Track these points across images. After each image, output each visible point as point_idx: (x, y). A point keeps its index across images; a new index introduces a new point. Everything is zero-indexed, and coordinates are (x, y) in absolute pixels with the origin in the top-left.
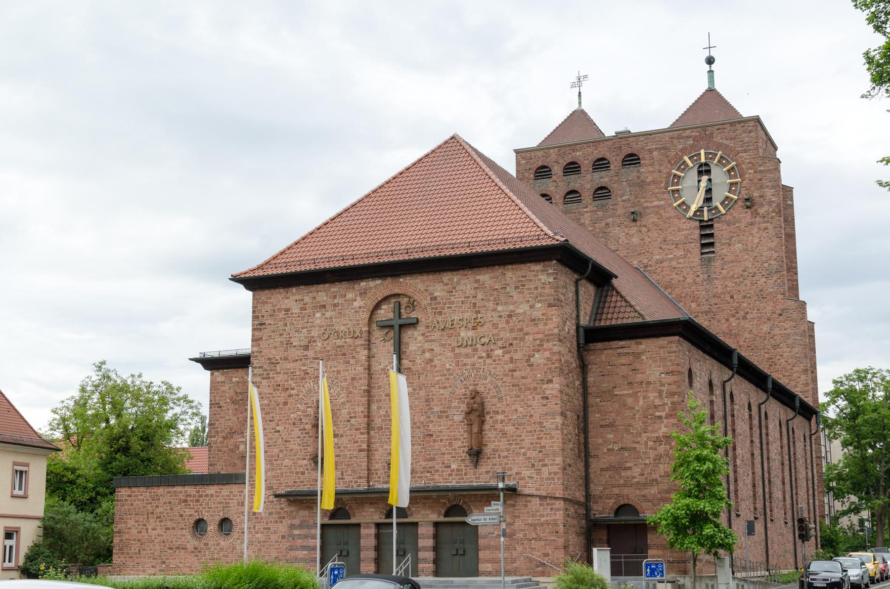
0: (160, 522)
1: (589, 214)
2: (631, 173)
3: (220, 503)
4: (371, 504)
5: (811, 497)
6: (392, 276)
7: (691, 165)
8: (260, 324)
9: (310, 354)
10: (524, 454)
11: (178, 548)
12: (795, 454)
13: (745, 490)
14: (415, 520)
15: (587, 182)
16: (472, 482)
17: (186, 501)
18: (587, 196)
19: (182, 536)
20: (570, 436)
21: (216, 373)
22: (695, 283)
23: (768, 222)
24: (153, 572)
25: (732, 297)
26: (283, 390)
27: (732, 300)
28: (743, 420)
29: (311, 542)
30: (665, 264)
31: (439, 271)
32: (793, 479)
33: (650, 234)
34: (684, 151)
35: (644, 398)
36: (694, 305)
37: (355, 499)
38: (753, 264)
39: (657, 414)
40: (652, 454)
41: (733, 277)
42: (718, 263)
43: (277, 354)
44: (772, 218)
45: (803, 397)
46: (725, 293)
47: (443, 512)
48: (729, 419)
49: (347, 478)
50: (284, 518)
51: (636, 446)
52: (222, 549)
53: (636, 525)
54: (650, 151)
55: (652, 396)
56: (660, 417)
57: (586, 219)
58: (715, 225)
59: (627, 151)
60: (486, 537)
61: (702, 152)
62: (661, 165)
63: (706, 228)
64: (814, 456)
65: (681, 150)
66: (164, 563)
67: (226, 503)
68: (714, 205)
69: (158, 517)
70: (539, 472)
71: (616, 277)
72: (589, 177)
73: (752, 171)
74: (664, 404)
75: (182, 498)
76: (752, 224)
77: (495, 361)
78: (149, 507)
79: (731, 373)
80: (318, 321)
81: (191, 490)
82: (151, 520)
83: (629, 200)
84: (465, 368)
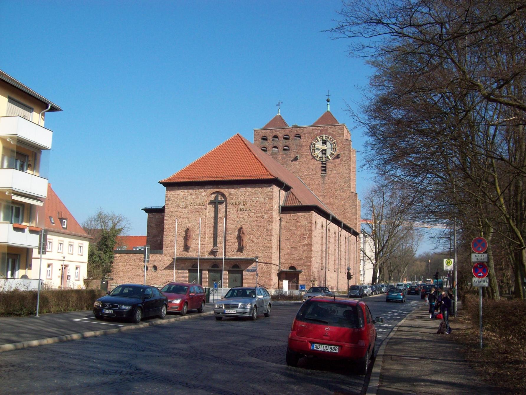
2: (297, 141)
9: (186, 210)
13: (332, 262)
15: (281, 143)
18: (281, 149)
22: (318, 184)
29: (185, 275)
30: (308, 176)
34: (317, 135)
36: (318, 192)
40: (302, 250)
42: (327, 178)
43: (173, 210)
45: (354, 229)
48: (328, 238)
54: (305, 134)
55: (303, 230)
57: (280, 157)
58: (327, 163)
59: (296, 133)
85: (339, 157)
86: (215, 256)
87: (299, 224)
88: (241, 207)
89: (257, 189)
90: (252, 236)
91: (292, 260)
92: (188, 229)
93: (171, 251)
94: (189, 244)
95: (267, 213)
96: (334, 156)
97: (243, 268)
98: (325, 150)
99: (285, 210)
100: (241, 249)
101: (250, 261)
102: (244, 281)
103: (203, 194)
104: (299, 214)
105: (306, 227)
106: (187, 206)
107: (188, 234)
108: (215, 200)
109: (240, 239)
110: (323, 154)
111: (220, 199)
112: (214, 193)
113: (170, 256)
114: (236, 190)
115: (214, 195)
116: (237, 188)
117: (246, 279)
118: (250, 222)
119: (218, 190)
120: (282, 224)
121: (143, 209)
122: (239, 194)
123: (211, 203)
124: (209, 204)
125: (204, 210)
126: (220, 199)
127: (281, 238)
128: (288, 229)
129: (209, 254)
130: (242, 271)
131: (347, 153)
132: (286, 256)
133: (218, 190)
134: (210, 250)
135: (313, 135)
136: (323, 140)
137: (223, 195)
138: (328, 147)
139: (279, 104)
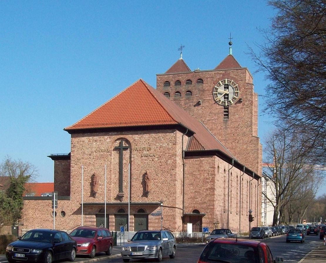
1: (183, 101)
2: (200, 86)
5: (256, 207)
7: (222, 84)
9: (92, 157)
10: (164, 193)
12: (252, 192)
15: (183, 88)
19: (48, 216)
20: (179, 188)
21: (56, 161)
23: (248, 108)
25: (234, 135)
27: (234, 136)
28: (235, 182)
29: (93, 220)
30: (211, 121)
32: (251, 201)
33: (205, 110)
34: (219, 79)
35: (203, 175)
36: (220, 137)
38: (242, 123)
39: (207, 181)
40: (205, 194)
41: (234, 127)
43: (79, 156)
44: (250, 106)
46: (231, 133)
47: (137, 211)
51: (200, 191)
52: (61, 221)
53: (190, 216)
54: (207, 78)
55: (206, 175)
56: (208, 182)
57: (182, 103)
59: (198, 77)
60: (151, 219)
62: (211, 84)
63: (226, 108)
64: (258, 193)
65: (218, 79)
66: (42, 225)
69: (39, 210)
71: (195, 133)
72: (184, 87)
73: (243, 88)
74: (209, 178)
76: (242, 108)
77: (155, 162)
78: (36, 207)
79: (232, 166)
82: (37, 211)
83: (198, 96)
84: (145, 164)
85: (241, 102)
86: (121, 201)
87: (202, 169)
88: (145, 152)
89: (160, 135)
92: (94, 175)
93: (78, 197)
95: (170, 158)
96: (236, 101)
97: (148, 212)
98: (228, 95)
99: (188, 155)
100: (146, 194)
103: (108, 140)
104: (202, 159)
106: (92, 152)
107: (94, 180)
108: (120, 146)
109: (144, 184)
110: (225, 98)
111: (124, 145)
112: (118, 139)
114: (140, 136)
115: (118, 142)
116: (141, 134)
118: (155, 167)
120: (186, 169)
121: (49, 157)
122: (143, 140)
123: (116, 149)
124: (114, 150)
125: (109, 157)
126: (124, 145)
127: (185, 182)
128: (192, 174)
129: (115, 199)
130: (148, 215)
131: (249, 97)
134: (116, 196)
135: (215, 80)
136: (225, 85)
137: (127, 141)
138: (230, 91)
139: (181, 48)
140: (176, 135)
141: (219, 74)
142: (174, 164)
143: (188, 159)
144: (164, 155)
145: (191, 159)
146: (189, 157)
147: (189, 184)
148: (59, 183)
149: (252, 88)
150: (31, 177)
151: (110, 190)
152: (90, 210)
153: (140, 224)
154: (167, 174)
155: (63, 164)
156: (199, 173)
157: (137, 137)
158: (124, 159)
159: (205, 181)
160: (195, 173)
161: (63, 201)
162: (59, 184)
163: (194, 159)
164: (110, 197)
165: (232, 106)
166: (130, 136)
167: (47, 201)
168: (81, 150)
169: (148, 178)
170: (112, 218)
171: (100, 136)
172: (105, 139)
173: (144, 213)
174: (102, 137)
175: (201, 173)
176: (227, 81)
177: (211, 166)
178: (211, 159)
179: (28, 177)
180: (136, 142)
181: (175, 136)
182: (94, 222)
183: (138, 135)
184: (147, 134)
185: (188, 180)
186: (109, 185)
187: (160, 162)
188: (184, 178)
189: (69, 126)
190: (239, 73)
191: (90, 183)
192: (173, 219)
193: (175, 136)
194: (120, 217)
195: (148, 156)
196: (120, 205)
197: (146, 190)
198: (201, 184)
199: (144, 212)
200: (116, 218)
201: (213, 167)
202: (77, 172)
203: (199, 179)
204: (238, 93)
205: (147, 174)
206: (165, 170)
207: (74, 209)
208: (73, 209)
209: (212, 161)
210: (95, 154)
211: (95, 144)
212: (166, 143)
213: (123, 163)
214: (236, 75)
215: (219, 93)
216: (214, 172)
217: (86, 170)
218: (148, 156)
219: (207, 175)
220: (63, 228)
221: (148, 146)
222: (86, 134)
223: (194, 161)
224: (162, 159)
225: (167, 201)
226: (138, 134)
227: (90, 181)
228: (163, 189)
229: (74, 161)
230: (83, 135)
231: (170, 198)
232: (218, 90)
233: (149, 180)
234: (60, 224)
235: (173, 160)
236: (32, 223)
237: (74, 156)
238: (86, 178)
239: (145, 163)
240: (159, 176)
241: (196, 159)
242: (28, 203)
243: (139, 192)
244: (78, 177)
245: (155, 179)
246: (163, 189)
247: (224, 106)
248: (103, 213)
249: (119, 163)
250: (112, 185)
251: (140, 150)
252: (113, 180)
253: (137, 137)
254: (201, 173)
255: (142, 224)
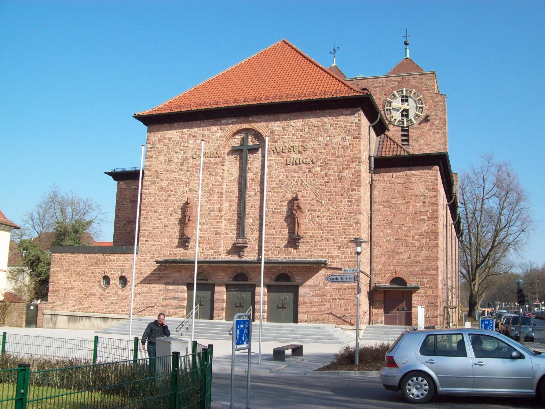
0: (79, 276)
3: (119, 266)
4: (223, 270)
6: (243, 116)
7: (398, 96)
8: (151, 148)
9: (185, 168)
11: (90, 294)
14: (253, 283)
16: (295, 258)
17: (96, 264)
21: (121, 183)
23: (439, 129)
24: (73, 310)
26: (164, 191)
29: (181, 295)
31: (277, 113)
34: (393, 88)
37: (212, 267)
39: (422, 217)
40: (417, 244)
43: (159, 167)
44: (441, 127)
47: (274, 277)
49: (207, 253)
50: (161, 277)
51: (407, 238)
52: (119, 297)
53: (385, 291)
54: (375, 87)
56: (424, 219)
61: (404, 89)
65: (392, 88)
66: (81, 304)
67: (123, 266)
68: (409, 118)
69: (78, 274)
70: (344, 252)
75: (94, 261)
76: (430, 130)
78: (72, 266)
80: (191, 146)
81: (101, 256)
82: (74, 275)
85: (429, 121)
86: (240, 256)
87: (410, 192)
88: (293, 156)
89: (326, 119)
90: (319, 213)
91: (398, 264)
92: (187, 203)
93: (153, 248)
94: (188, 232)
95: (348, 167)
96: (420, 120)
97: (298, 280)
98: (407, 111)
99: (382, 164)
100: (294, 241)
101: (312, 268)
102: (300, 308)
103: (218, 135)
104: (409, 173)
105: (426, 198)
106: (186, 158)
107: (187, 214)
108: (241, 145)
109: (292, 220)
110: (403, 116)
111: (250, 143)
112: (239, 132)
113: (152, 257)
114: (284, 123)
115: (239, 137)
116: (286, 120)
117: (304, 303)
118: (314, 185)
119: (247, 126)
120: (375, 193)
121: (109, 174)
122: (289, 131)
123: (234, 151)
124: (229, 153)
125: (220, 167)
126: (250, 143)
127: (374, 220)
128: (388, 203)
129: (229, 252)
130: (297, 287)
131: (440, 113)
132: (384, 257)
133: (247, 126)
134: (230, 245)
135: (387, 89)
136: (403, 97)
137: (258, 136)
138: (411, 105)
139: (334, 51)
140: (359, 120)
141: (393, 81)
142: (357, 178)
143: (380, 174)
144: (335, 161)
145: (387, 174)
146: (383, 169)
147: (382, 224)
148: (124, 224)
149: (444, 100)
150: (93, 224)
151: (219, 234)
152: (177, 275)
153: (237, 305)
154: (340, 200)
155: (133, 187)
156: (404, 202)
157: (278, 126)
158: (249, 171)
159: (417, 217)
160: (396, 202)
161: (125, 255)
162: (123, 225)
163: (394, 174)
164: (217, 247)
165: (414, 128)
166: (264, 124)
167: (93, 255)
168: (165, 155)
169: (299, 208)
170: (219, 292)
171: (204, 127)
172: (214, 131)
173: (289, 283)
174: (207, 128)
175: (408, 202)
176: (406, 91)
177: (429, 187)
178: (428, 173)
179: (89, 223)
180: (276, 135)
181: (357, 120)
182: (184, 299)
183: (279, 122)
184: (299, 120)
185: (381, 215)
186: (218, 222)
187: (326, 174)
188: (373, 213)
189: (146, 110)
190: (424, 80)
191: (178, 220)
192: (353, 295)
193: (357, 120)
194: (238, 291)
195: (300, 164)
196: (237, 265)
197: (294, 233)
198: (408, 224)
199: (290, 281)
200: (229, 293)
201: (433, 189)
202: (155, 199)
203: (402, 213)
204: (422, 107)
205: (297, 200)
206: (335, 192)
207: (145, 273)
208: (142, 271)
209: (432, 176)
210: (191, 161)
211: (192, 142)
212: (339, 135)
213: (248, 178)
214: (419, 83)
215: (394, 109)
216: (437, 199)
217: (173, 193)
218: (300, 164)
219: (421, 206)
220: (120, 310)
221: (301, 144)
222: (176, 125)
223: (394, 176)
224: (329, 169)
225: (340, 257)
226: (280, 121)
227: (180, 216)
228: (331, 230)
229: (151, 176)
230: (171, 127)
231: (348, 250)
232: (392, 104)
233: (302, 212)
234: (115, 301)
235: (353, 170)
236: (64, 299)
237: (150, 166)
238: (172, 209)
239: (294, 177)
240: (323, 204)
241: (398, 174)
242: (60, 259)
243: (278, 238)
244: (156, 208)
245: (314, 211)
246: (331, 230)
247: (402, 127)
248: (200, 282)
249: (239, 179)
250: (223, 224)
251: (284, 151)
252: (225, 214)
253: (278, 126)
254: (408, 202)
255: (284, 306)
